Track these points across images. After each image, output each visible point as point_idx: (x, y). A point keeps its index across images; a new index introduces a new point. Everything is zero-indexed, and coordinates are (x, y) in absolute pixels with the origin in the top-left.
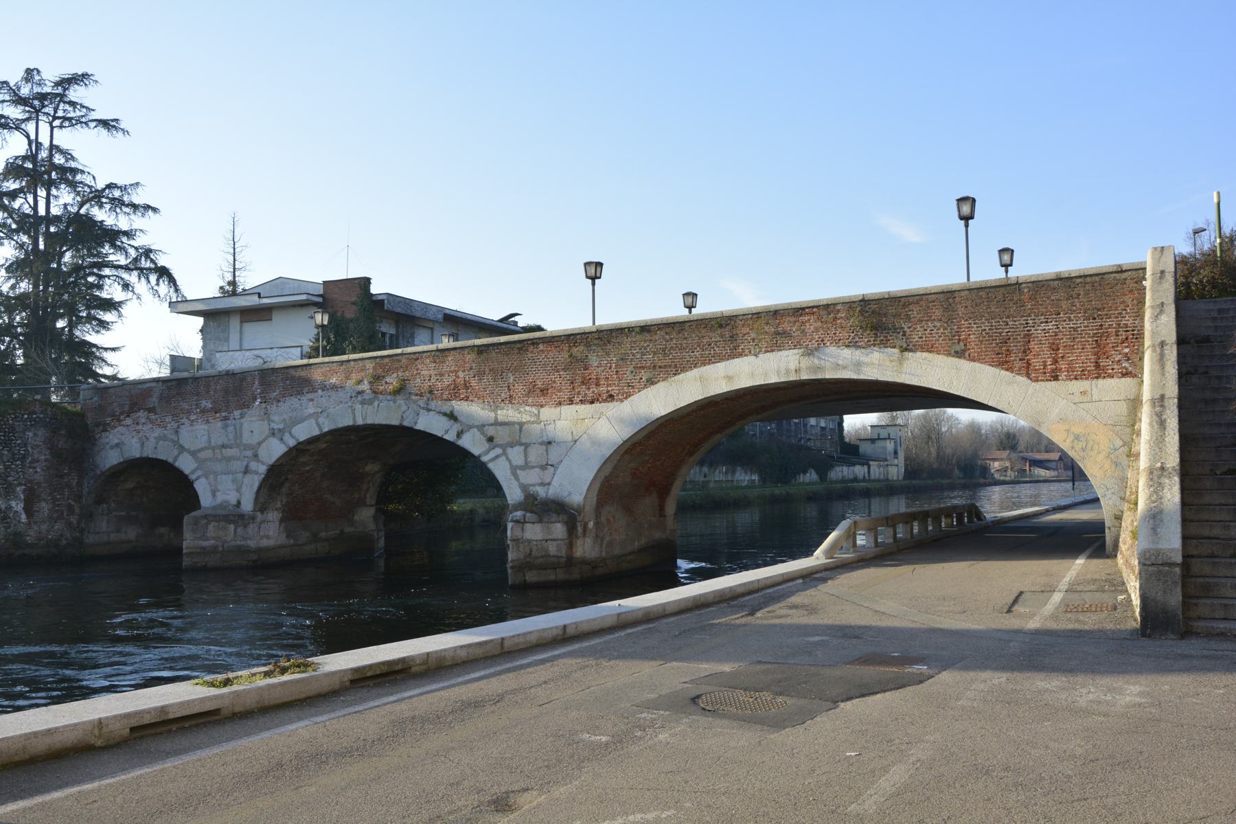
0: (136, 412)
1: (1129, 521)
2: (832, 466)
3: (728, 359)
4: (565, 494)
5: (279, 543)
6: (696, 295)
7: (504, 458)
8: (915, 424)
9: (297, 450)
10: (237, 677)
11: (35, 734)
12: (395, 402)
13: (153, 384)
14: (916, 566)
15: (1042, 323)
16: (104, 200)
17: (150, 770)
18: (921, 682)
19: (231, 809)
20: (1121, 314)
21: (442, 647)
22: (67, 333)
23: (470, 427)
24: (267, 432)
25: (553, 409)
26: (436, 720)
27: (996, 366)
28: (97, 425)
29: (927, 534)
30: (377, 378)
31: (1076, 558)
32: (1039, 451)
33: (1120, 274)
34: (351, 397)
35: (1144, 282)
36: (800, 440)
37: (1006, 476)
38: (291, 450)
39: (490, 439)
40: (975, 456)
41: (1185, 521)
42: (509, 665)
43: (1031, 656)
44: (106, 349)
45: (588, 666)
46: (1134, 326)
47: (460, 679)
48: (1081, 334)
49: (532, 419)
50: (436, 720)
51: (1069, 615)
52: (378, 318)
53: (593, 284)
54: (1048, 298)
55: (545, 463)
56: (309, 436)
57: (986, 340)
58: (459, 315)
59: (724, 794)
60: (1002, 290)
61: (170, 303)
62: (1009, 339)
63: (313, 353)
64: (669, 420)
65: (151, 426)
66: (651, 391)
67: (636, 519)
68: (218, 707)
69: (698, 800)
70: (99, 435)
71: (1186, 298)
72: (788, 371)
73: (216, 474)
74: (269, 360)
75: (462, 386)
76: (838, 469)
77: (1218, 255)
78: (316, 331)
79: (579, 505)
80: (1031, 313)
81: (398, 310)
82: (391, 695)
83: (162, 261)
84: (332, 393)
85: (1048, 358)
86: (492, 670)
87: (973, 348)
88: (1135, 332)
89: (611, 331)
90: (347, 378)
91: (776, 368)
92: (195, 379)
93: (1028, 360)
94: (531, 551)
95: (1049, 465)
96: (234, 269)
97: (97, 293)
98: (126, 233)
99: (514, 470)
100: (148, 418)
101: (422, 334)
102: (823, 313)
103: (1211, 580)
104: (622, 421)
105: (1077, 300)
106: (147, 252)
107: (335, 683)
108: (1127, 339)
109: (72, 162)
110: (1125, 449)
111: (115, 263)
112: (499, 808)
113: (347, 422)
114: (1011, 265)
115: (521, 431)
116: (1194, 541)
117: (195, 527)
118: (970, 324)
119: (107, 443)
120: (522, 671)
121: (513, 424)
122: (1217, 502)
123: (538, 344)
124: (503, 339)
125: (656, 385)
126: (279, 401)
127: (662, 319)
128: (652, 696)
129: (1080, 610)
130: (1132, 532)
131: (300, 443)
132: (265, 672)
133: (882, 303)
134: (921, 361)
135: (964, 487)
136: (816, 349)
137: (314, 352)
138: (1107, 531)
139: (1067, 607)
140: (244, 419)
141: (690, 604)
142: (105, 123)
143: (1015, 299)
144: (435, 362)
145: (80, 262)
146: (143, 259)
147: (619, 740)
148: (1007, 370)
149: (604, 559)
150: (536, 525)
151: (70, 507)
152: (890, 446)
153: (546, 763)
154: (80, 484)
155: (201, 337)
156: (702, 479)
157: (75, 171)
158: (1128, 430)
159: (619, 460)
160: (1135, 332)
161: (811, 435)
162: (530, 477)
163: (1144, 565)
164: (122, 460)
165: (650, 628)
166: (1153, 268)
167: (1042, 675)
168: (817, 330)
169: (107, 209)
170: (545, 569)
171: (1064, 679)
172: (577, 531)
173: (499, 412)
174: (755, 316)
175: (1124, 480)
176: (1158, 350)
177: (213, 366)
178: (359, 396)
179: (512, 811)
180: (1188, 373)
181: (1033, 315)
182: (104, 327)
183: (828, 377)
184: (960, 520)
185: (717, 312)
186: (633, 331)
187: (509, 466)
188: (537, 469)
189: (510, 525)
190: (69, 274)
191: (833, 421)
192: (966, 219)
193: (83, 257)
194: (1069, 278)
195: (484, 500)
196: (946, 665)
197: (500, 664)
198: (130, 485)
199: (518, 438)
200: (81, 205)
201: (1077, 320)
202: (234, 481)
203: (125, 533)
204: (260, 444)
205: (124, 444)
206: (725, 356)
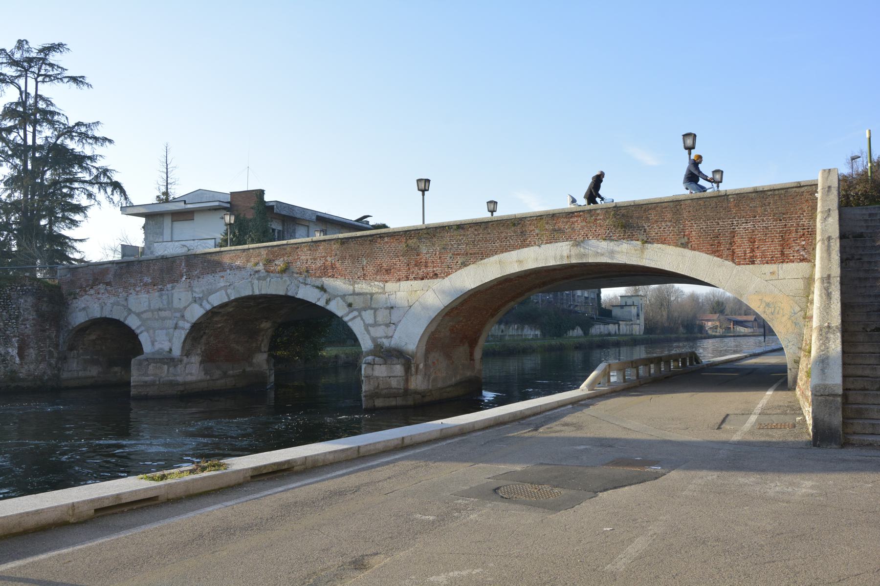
0: (97, 285)
1: (804, 365)
3: (519, 249)
4: (403, 344)
5: (199, 378)
6: (496, 203)
7: (359, 318)
8: (652, 295)
9: (212, 312)
10: (170, 474)
11: (28, 514)
12: (282, 279)
13: (110, 265)
14: (653, 396)
15: (743, 223)
16: (74, 134)
17: (109, 539)
18: (656, 478)
22: (48, 229)
23: (335, 296)
28: (70, 294)
29: (660, 373)
30: (269, 262)
31: (767, 390)
32: (740, 314)
33: (799, 189)
34: (251, 275)
35: (816, 194)
37: (716, 332)
38: (207, 313)
39: (350, 305)
40: (695, 317)
41: (844, 364)
42: (363, 466)
44: (76, 240)
45: (419, 467)
48: (771, 231)
49: (380, 291)
51: (761, 431)
52: (269, 219)
53: (423, 195)
54: (748, 205)
55: (388, 322)
57: (703, 236)
58: (327, 216)
60: (715, 199)
61: (121, 207)
62: (720, 235)
63: (224, 244)
64: (477, 292)
65: (108, 295)
67: (453, 362)
68: (157, 495)
70: (71, 302)
72: (562, 257)
74: (192, 248)
75: (330, 267)
76: (597, 327)
77: (869, 175)
78: (225, 228)
79: (413, 352)
81: (284, 213)
83: (115, 178)
84: (237, 272)
85: (748, 248)
86: (351, 469)
87: (694, 241)
89: (436, 228)
90: (248, 261)
93: (733, 249)
94: (378, 385)
95: (746, 324)
96: (167, 183)
99: (367, 327)
100: (106, 289)
101: (301, 230)
102: (587, 215)
104: (443, 292)
105: (768, 207)
106: (105, 171)
108: (804, 234)
109: (51, 107)
110: (802, 313)
111: (82, 179)
112: (357, 566)
113: (247, 292)
118: (692, 224)
120: (373, 470)
121: (366, 294)
123: (384, 237)
124: (359, 234)
125: (468, 267)
126: (199, 277)
127: (473, 220)
128: (466, 488)
130: (807, 372)
131: (214, 308)
134: (657, 250)
135: (687, 340)
136: (582, 242)
137: (225, 243)
139: (760, 425)
140: (174, 290)
141: (492, 423)
142: (74, 79)
143: (724, 206)
144: (310, 250)
145: (57, 178)
146: (102, 176)
149: (431, 391)
151: (50, 352)
152: (634, 310)
153: (390, 535)
154: (57, 336)
155: (143, 232)
156: (500, 333)
157: (53, 113)
158: (804, 300)
160: (809, 230)
161: (578, 302)
162: (378, 332)
163: (816, 395)
164: (87, 319)
165: (463, 440)
167: (743, 473)
168: (582, 228)
169: (76, 141)
170: (389, 397)
171: (758, 476)
173: (356, 286)
174: (539, 218)
175: (801, 335)
176: (826, 243)
177: (152, 253)
178: (256, 274)
182: (74, 225)
183: (590, 261)
184: (684, 363)
186: (452, 228)
187: (363, 324)
188: (383, 326)
189: (363, 366)
190: (49, 187)
193: (59, 175)
194: (763, 192)
195: (345, 348)
196: (674, 465)
198: (93, 337)
199: (369, 304)
200: (58, 138)
201: (768, 222)
202: (167, 334)
203: (90, 371)
204: (185, 308)
205: (88, 307)
206: (517, 246)
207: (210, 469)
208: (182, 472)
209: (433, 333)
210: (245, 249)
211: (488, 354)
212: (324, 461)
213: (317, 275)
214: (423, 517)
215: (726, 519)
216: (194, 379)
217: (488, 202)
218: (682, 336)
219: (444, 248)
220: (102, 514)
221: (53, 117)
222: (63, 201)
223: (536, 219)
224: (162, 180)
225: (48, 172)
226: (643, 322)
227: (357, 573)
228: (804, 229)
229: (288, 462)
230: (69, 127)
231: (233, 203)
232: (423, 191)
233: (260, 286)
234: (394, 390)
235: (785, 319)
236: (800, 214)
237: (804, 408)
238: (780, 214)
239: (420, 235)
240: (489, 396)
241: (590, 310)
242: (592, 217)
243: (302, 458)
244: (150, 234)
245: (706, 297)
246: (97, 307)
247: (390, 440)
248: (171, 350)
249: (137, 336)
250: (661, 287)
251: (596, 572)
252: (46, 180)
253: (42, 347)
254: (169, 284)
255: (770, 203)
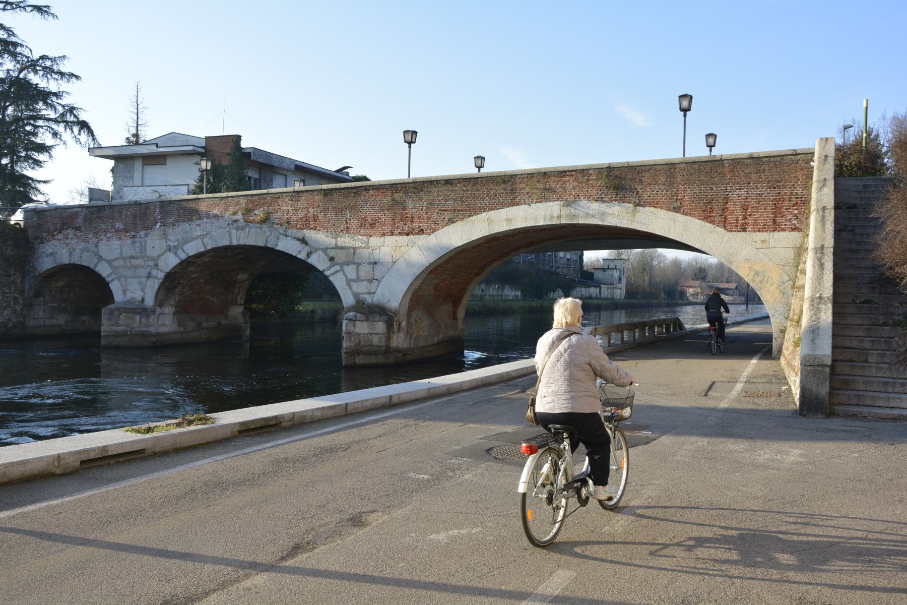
0: (66, 229)
1: (791, 334)
2: (574, 287)
3: (508, 207)
4: (386, 301)
5: (173, 330)
6: (484, 158)
7: (341, 273)
8: (635, 259)
9: (187, 262)
10: (156, 427)
11: (12, 464)
12: (261, 229)
13: (79, 209)
14: (638, 361)
15: (737, 189)
16: (38, 68)
17: (98, 492)
18: (647, 443)
19: (161, 520)
20: (793, 185)
21: (304, 409)
22: (9, 168)
23: (317, 250)
24: (165, 248)
25: (379, 238)
26: (302, 460)
27: (702, 219)
28: (37, 238)
29: (645, 338)
30: (248, 211)
31: (751, 359)
32: (722, 282)
33: (795, 157)
34: (229, 224)
35: (811, 163)
36: (552, 268)
37: (697, 299)
38: (182, 262)
39: (332, 259)
40: (676, 283)
41: (835, 335)
42: (352, 423)
43: (723, 427)
44: (39, 182)
45: (409, 425)
46: (802, 195)
47: (318, 432)
48: (764, 199)
49: (363, 245)
50: (302, 460)
51: (748, 399)
52: (246, 166)
53: (410, 147)
54: (743, 171)
55: (371, 278)
56: (196, 252)
57: (696, 201)
58: (306, 166)
59: (515, 517)
60: (710, 164)
61: (89, 148)
62: (713, 200)
63: (197, 190)
64: (463, 250)
65: (77, 240)
66: (451, 228)
67: (436, 321)
68: (143, 448)
69: (497, 521)
70: (37, 246)
71: (839, 176)
72: (552, 217)
73: (126, 278)
74: (164, 194)
75: (312, 219)
76: (578, 289)
77: (864, 145)
78: (199, 174)
79: (395, 309)
80: (730, 182)
81: (262, 160)
82: (269, 442)
83: (82, 117)
84: (214, 221)
85: (740, 215)
86: (340, 426)
87: (687, 206)
88: (803, 199)
89: (424, 182)
90: (226, 210)
91: (543, 215)
92: (111, 207)
93: (726, 216)
94: (360, 342)
95: (728, 292)
96: (138, 125)
97: (33, 139)
98: (55, 94)
99: (349, 282)
100: (75, 234)
101: (278, 179)
102: (579, 175)
103: (849, 378)
104: (429, 249)
105: (763, 174)
106: (72, 110)
107: (228, 433)
108: (797, 203)
109: (13, 37)
110: (791, 283)
111: (46, 116)
112: (355, 523)
113: (225, 242)
114: (714, 146)
115: (354, 253)
116: (838, 350)
117: (110, 317)
118: (685, 188)
119: (44, 252)
120: (362, 428)
121: (349, 248)
122: (856, 323)
123: (369, 190)
124: (343, 185)
125: (455, 224)
126: (174, 225)
127: (461, 175)
128: (458, 448)
129: (756, 396)
130: (794, 342)
131: (189, 257)
132: (176, 423)
133: (623, 171)
134: (649, 214)
135: (668, 306)
136: (573, 202)
137: (200, 190)
138: (774, 340)
139: (746, 394)
140: (148, 238)
141: (479, 384)
142: (38, 9)
143: (719, 171)
144: (292, 200)
145: (20, 115)
146: (68, 114)
147: (437, 478)
148: (710, 222)
149: (413, 349)
150: (364, 322)
151: (15, 299)
152: (616, 274)
153: (386, 493)
154: (23, 282)
155: (111, 175)
156: (480, 293)
157: (15, 45)
158: (794, 269)
159: (426, 277)
160: (803, 199)
161: (560, 264)
162: (361, 288)
163: (805, 365)
164: (55, 265)
165: (451, 400)
166: (820, 153)
167: (732, 440)
168: (574, 188)
169: (41, 75)
170: (370, 355)
171: (747, 443)
172: (393, 328)
173: (339, 239)
174: (530, 176)
175: (788, 306)
176: (821, 213)
177: (121, 197)
178: (235, 223)
179: (365, 526)
180: (840, 230)
181: (731, 183)
182: (38, 165)
183: (581, 222)
184: (668, 329)
185: (502, 172)
186: (440, 183)
187: (345, 279)
188: (365, 282)
189: (345, 322)
190: (11, 123)
191: (576, 254)
192: (685, 110)
193: (21, 111)
194: (759, 158)
195: (322, 303)
196: (665, 430)
197: (345, 422)
198: (60, 284)
199: (352, 259)
200: (21, 71)
201: (762, 189)
202: (140, 283)
203: (57, 319)
204: (159, 256)
205: (56, 253)
206: (506, 204)
207: (197, 423)
208: (168, 425)
209: (417, 291)
210: (223, 197)
211: (470, 314)
212: (312, 417)
213: (299, 227)
214: (418, 476)
215: (719, 485)
216: (167, 330)
217: (475, 158)
218: (663, 301)
219: (431, 204)
220: (89, 466)
221: (16, 49)
222: (26, 140)
223: (527, 177)
224: (132, 121)
225: (10, 107)
226: (625, 286)
227: (355, 530)
228: (797, 198)
229: (276, 417)
230: (32, 60)
231: (207, 148)
232: (410, 143)
233: (238, 236)
234: (375, 348)
235: (773, 288)
236: (795, 182)
237: (789, 378)
238: (774, 181)
239: (407, 188)
240: (472, 355)
241: (572, 272)
242: (584, 176)
243: (290, 414)
244: (119, 177)
245: (688, 262)
246: (66, 252)
247: (377, 398)
248: (143, 299)
249: (108, 284)
250: (643, 251)
251: (595, 533)
252: (8, 116)
253: (6, 293)
254: (142, 231)
255: (765, 170)
